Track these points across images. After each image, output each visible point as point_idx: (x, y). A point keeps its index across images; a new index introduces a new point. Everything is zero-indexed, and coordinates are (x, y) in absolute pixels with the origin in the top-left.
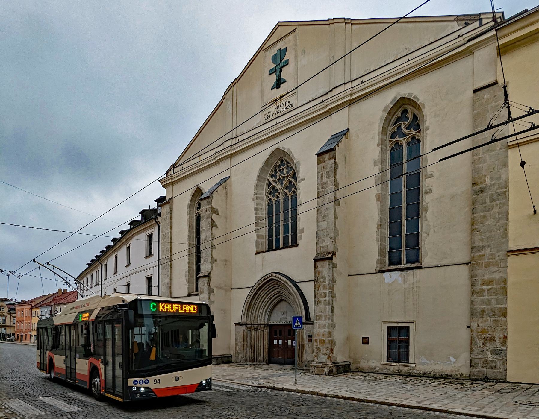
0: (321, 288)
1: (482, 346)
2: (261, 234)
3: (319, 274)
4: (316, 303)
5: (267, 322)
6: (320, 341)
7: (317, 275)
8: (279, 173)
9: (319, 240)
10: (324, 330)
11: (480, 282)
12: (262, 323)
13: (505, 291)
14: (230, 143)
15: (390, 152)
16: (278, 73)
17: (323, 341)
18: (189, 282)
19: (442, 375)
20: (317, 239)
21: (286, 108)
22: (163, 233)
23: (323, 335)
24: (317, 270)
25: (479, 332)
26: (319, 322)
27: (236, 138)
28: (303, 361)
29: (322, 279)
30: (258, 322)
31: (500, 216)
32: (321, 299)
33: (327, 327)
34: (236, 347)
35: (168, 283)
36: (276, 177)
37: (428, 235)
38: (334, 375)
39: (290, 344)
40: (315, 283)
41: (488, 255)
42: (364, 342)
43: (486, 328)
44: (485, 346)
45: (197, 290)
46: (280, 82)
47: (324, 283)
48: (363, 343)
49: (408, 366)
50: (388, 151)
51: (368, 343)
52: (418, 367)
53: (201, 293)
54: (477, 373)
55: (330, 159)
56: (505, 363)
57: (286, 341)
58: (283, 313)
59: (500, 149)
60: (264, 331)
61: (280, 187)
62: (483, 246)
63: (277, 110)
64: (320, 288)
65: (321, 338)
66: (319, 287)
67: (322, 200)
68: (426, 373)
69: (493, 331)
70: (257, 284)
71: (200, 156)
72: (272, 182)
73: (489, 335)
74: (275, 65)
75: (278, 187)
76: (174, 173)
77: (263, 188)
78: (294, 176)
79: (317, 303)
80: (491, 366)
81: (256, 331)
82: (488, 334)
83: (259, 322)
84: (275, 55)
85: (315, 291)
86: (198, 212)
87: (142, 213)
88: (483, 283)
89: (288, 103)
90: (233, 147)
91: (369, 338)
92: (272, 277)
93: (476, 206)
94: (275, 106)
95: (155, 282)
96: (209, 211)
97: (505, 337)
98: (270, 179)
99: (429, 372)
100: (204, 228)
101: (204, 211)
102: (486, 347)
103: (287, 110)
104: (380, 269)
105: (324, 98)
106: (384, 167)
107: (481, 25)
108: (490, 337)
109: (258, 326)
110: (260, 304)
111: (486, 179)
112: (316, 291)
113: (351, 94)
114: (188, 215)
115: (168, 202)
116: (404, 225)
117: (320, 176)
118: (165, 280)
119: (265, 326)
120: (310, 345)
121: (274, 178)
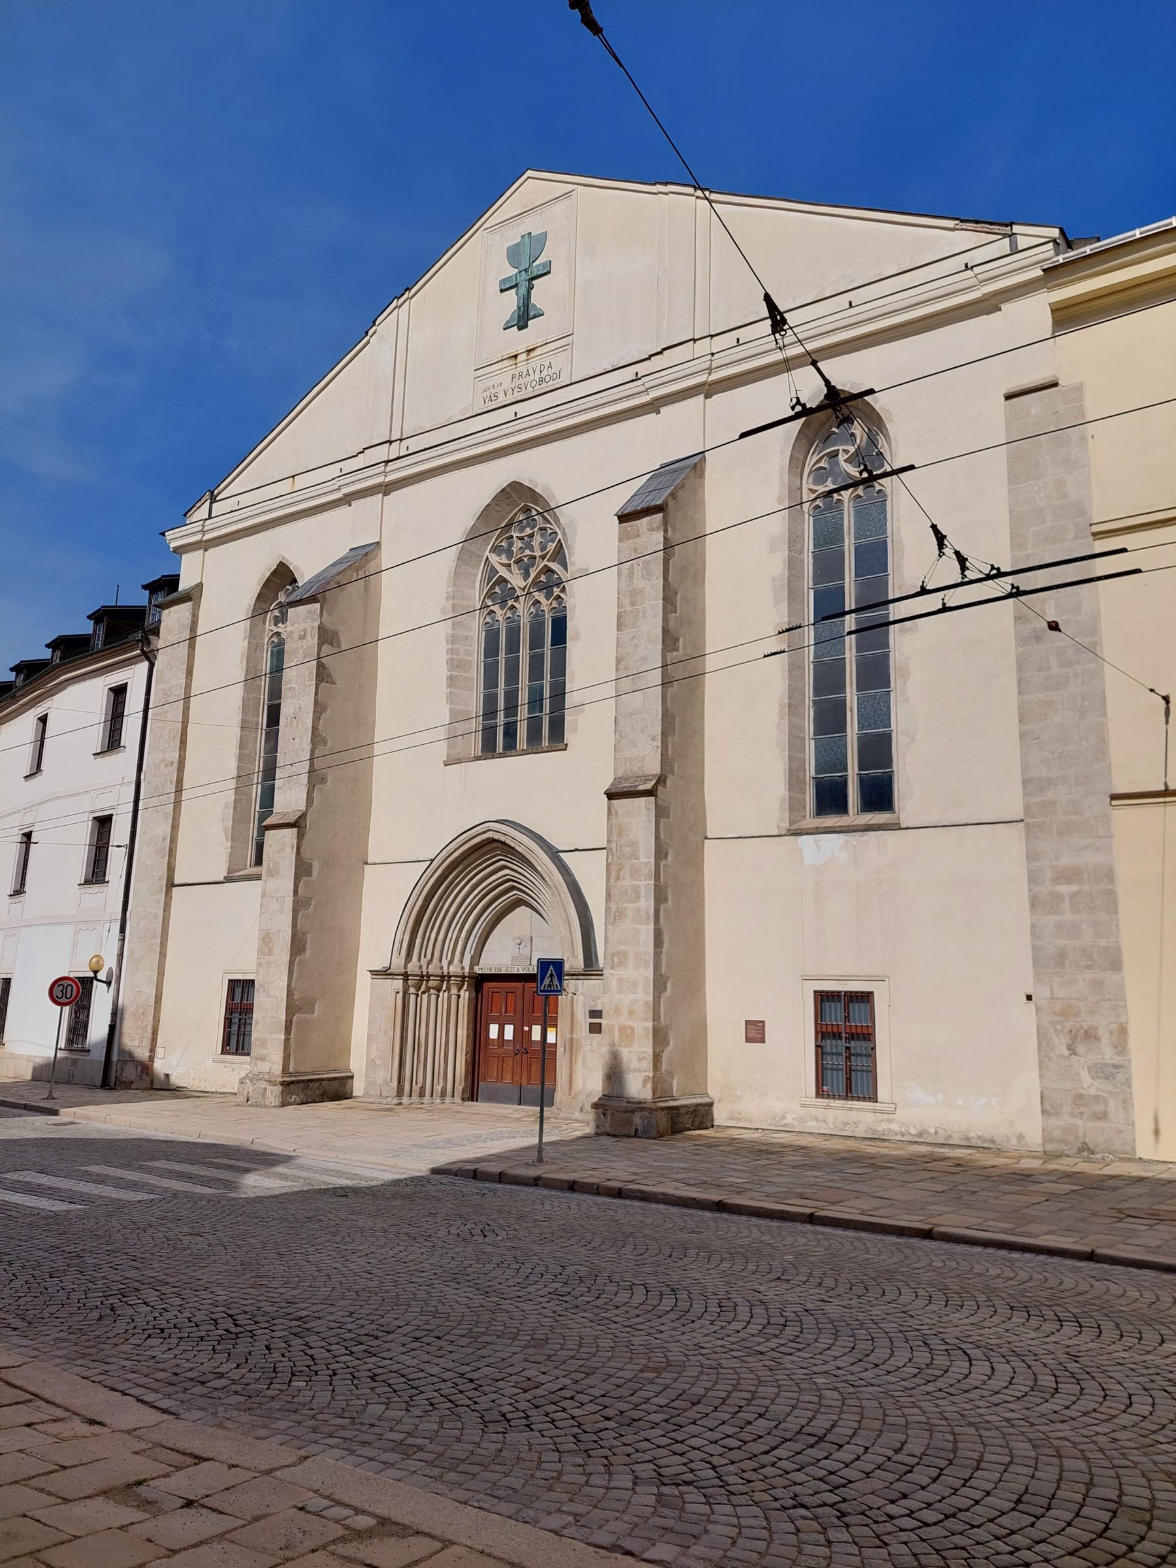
0: (626, 873)
1: (1066, 1053)
2: (463, 708)
3: (620, 835)
4: (612, 915)
5: (471, 967)
6: (623, 1029)
7: (615, 838)
8: (520, 545)
9: (623, 741)
10: (632, 997)
11: (1049, 874)
12: (453, 969)
13: (1111, 902)
14: (382, 453)
15: (811, 519)
16: (523, 290)
17: (629, 1031)
18: (235, 836)
19: (968, 1139)
20: (617, 736)
21: (542, 380)
22: (162, 686)
23: (631, 1013)
24: (614, 821)
25: (1055, 1014)
26: (619, 972)
27: (401, 440)
28: (573, 1094)
29: (627, 849)
30: (442, 968)
31: (1086, 704)
32: (625, 905)
33: (640, 989)
34: (369, 1046)
35: (164, 839)
36: (509, 553)
37: (913, 739)
38: (661, 1137)
39: (539, 1039)
40: (610, 858)
41: (1064, 804)
42: (750, 1035)
43: (1073, 1001)
44: (1075, 1054)
45: (259, 861)
46: (528, 314)
47: (635, 861)
48: (748, 1040)
49: (875, 1111)
50: (807, 516)
51: (762, 1040)
52: (901, 1114)
53: (271, 874)
54: (1059, 1132)
55: (653, 530)
56: (1127, 1104)
57: (526, 1029)
58: (519, 941)
59: (1076, 537)
60: (459, 996)
61: (522, 584)
62: (1049, 779)
63: (517, 382)
64: (622, 873)
65: (624, 1020)
66: (621, 869)
67: (631, 635)
68: (927, 1132)
69: (1092, 1013)
70: (444, 853)
71: (293, 477)
72: (498, 567)
73: (1083, 1021)
74: (516, 271)
75: (516, 580)
76: (210, 517)
77: (474, 582)
78: (559, 555)
79: (614, 916)
80: (1094, 1113)
81: (433, 997)
82: (1079, 1020)
83: (445, 969)
84: (518, 245)
85: (608, 880)
86: (276, 630)
87: (97, 617)
88: (1058, 878)
89: (546, 367)
90: (391, 466)
91: (763, 1022)
92: (490, 835)
93: (1027, 675)
94: (513, 372)
95: (119, 833)
96: (312, 638)
97: (1123, 1030)
98: (494, 559)
99: (932, 1131)
100: (293, 685)
101: (296, 637)
102: (1076, 1058)
103: (544, 384)
104: (790, 825)
105: (642, 369)
106: (797, 555)
107: (1015, 251)
108: (1086, 1028)
109: (442, 981)
110: (441, 937)
111: (1047, 608)
112: (612, 881)
113: (710, 370)
114: (245, 638)
115: (186, 598)
116: (851, 710)
117: (627, 571)
118: (153, 827)
119: (463, 982)
120: (595, 1042)
121: (504, 556)
